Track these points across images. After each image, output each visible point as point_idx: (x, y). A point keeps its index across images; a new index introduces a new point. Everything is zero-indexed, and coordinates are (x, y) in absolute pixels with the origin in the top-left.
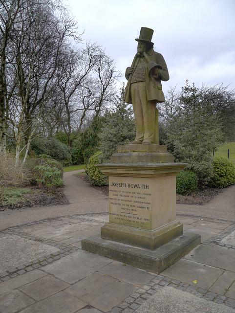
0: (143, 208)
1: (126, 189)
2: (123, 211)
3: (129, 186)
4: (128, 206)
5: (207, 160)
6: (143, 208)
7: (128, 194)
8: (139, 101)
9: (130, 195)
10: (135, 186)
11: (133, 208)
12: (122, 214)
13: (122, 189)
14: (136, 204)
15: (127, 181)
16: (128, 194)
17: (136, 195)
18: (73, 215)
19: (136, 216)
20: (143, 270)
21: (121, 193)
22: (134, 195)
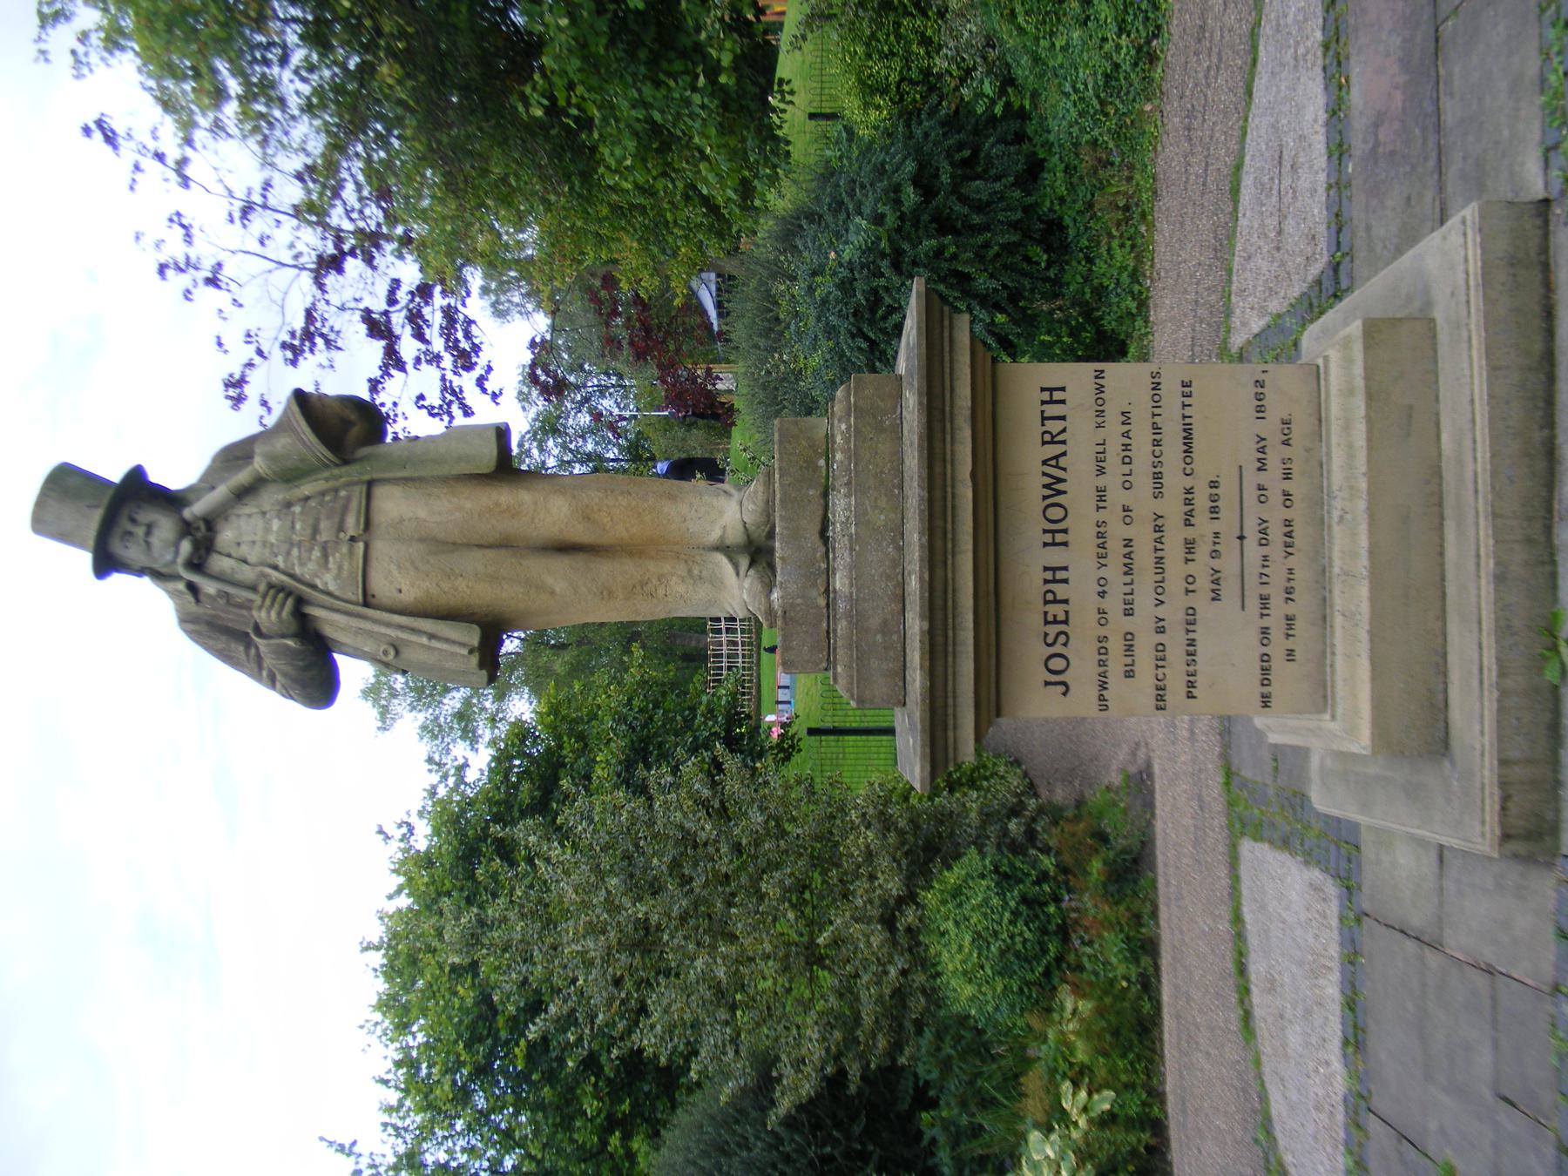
0: (1188, 431)
1: (1079, 558)
2: (1229, 589)
3: (1056, 536)
4: (1190, 545)
5: (1551, 45)
6: (1188, 431)
7: (1115, 547)
8: (491, 554)
9: (1116, 531)
10: (1054, 487)
11: (1201, 501)
12: (1253, 604)
13: (1080, 591)
14: (1174, 481)
15: (1029, 559)
16: (1276, 533)
17: (1112, 480)
18: (322, 335)
19: (1251, 478)
20: (913, 584)
21: (1114, 604)
22: (1116, 496)
